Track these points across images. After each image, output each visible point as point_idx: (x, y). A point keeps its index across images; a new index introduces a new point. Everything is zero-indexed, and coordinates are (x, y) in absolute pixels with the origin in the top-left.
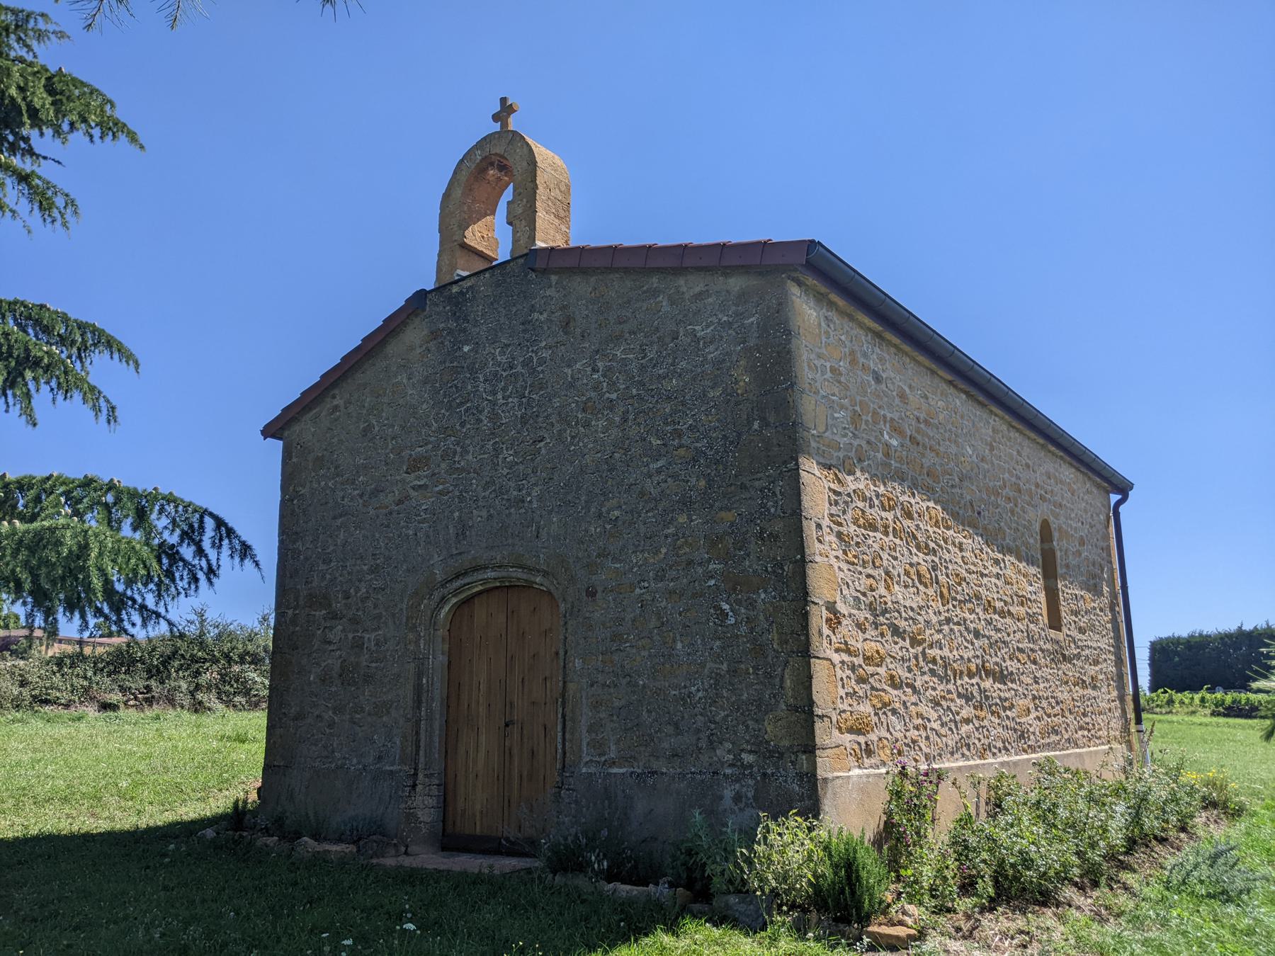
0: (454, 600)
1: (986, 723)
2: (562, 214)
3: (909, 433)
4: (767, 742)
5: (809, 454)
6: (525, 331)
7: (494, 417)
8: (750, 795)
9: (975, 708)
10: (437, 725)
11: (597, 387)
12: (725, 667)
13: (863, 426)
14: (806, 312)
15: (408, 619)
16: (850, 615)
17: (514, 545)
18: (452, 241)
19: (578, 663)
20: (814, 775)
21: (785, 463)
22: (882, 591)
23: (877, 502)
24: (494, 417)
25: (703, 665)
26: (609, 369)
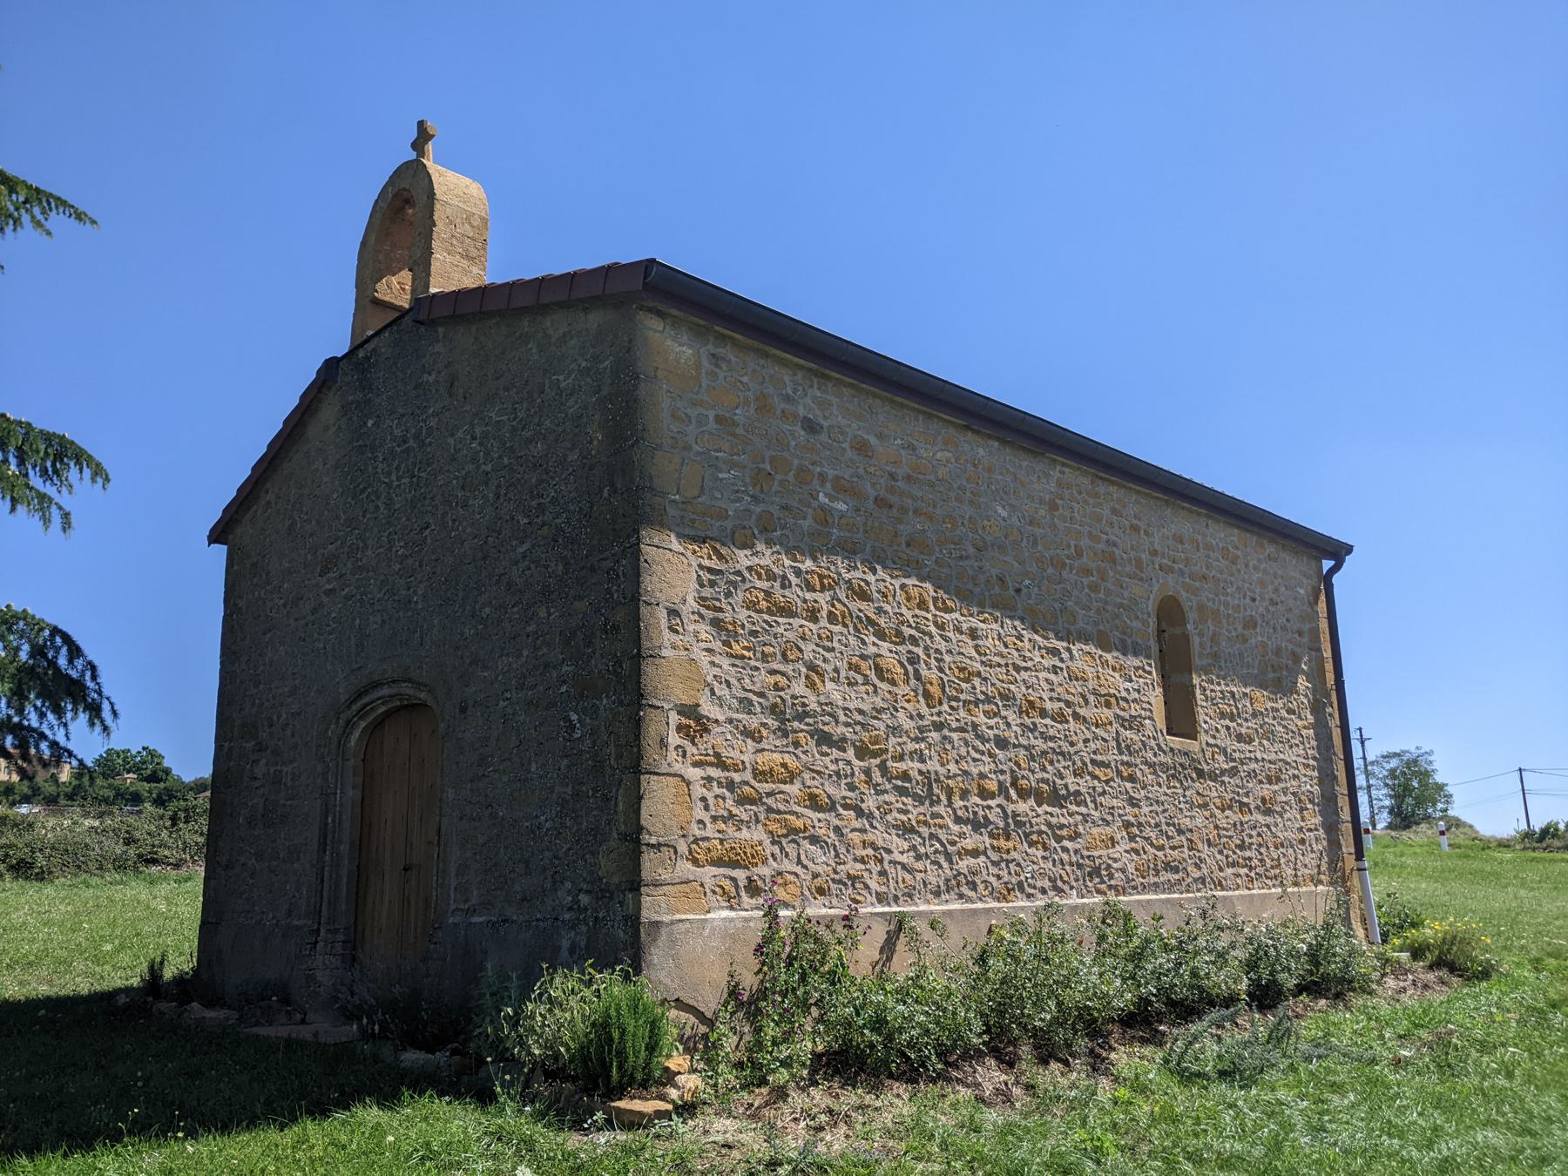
0: (363, 724)
1: (1014, 854)
2: (473, 252)
3: (872, 492)
4: (601, 879)
5: (662, 525)
6: (417, 397)
7: (389, 504)
8: (583, 944)
9: (991, 836)
10: (344, 872)
11: (474, 460)
12: (569, 790)
13: (776, 487)
14: (671, 347)
16: (730, 721)
18: (367, 301)
19: (450, 793)
20: (638, 918)
21: (629, 537)
22: (799, 688)
23: (794, 580)
24: (389, 504)
25: (552, 789)
26: (485, 435)
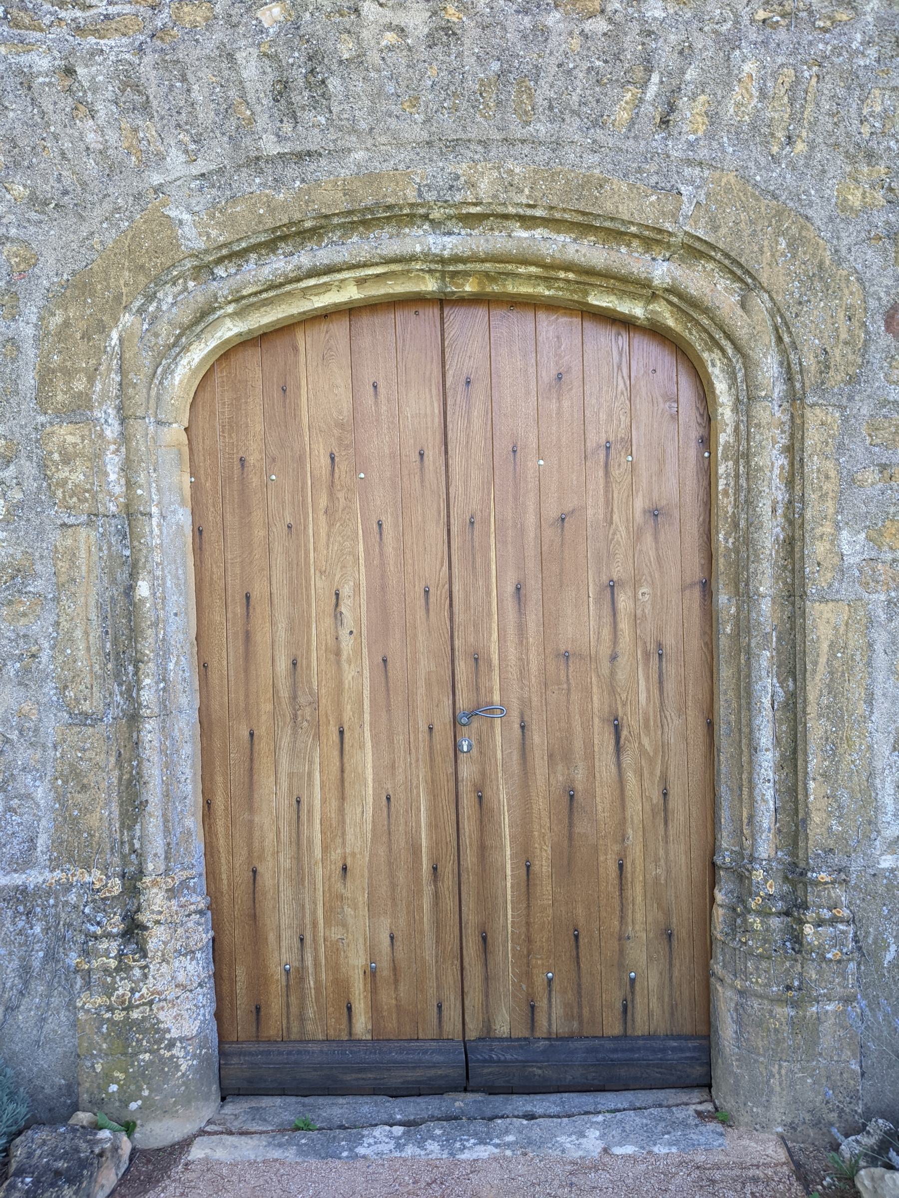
15: (46, 376)
17: (557, 144)
19: (852, 545)
